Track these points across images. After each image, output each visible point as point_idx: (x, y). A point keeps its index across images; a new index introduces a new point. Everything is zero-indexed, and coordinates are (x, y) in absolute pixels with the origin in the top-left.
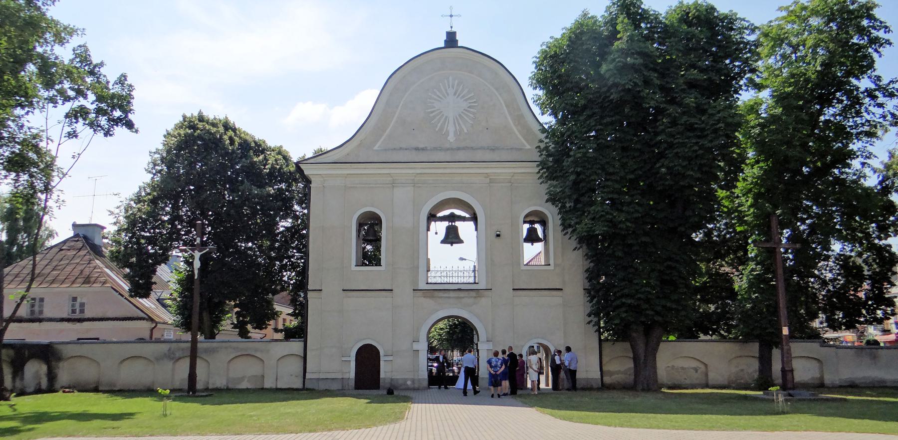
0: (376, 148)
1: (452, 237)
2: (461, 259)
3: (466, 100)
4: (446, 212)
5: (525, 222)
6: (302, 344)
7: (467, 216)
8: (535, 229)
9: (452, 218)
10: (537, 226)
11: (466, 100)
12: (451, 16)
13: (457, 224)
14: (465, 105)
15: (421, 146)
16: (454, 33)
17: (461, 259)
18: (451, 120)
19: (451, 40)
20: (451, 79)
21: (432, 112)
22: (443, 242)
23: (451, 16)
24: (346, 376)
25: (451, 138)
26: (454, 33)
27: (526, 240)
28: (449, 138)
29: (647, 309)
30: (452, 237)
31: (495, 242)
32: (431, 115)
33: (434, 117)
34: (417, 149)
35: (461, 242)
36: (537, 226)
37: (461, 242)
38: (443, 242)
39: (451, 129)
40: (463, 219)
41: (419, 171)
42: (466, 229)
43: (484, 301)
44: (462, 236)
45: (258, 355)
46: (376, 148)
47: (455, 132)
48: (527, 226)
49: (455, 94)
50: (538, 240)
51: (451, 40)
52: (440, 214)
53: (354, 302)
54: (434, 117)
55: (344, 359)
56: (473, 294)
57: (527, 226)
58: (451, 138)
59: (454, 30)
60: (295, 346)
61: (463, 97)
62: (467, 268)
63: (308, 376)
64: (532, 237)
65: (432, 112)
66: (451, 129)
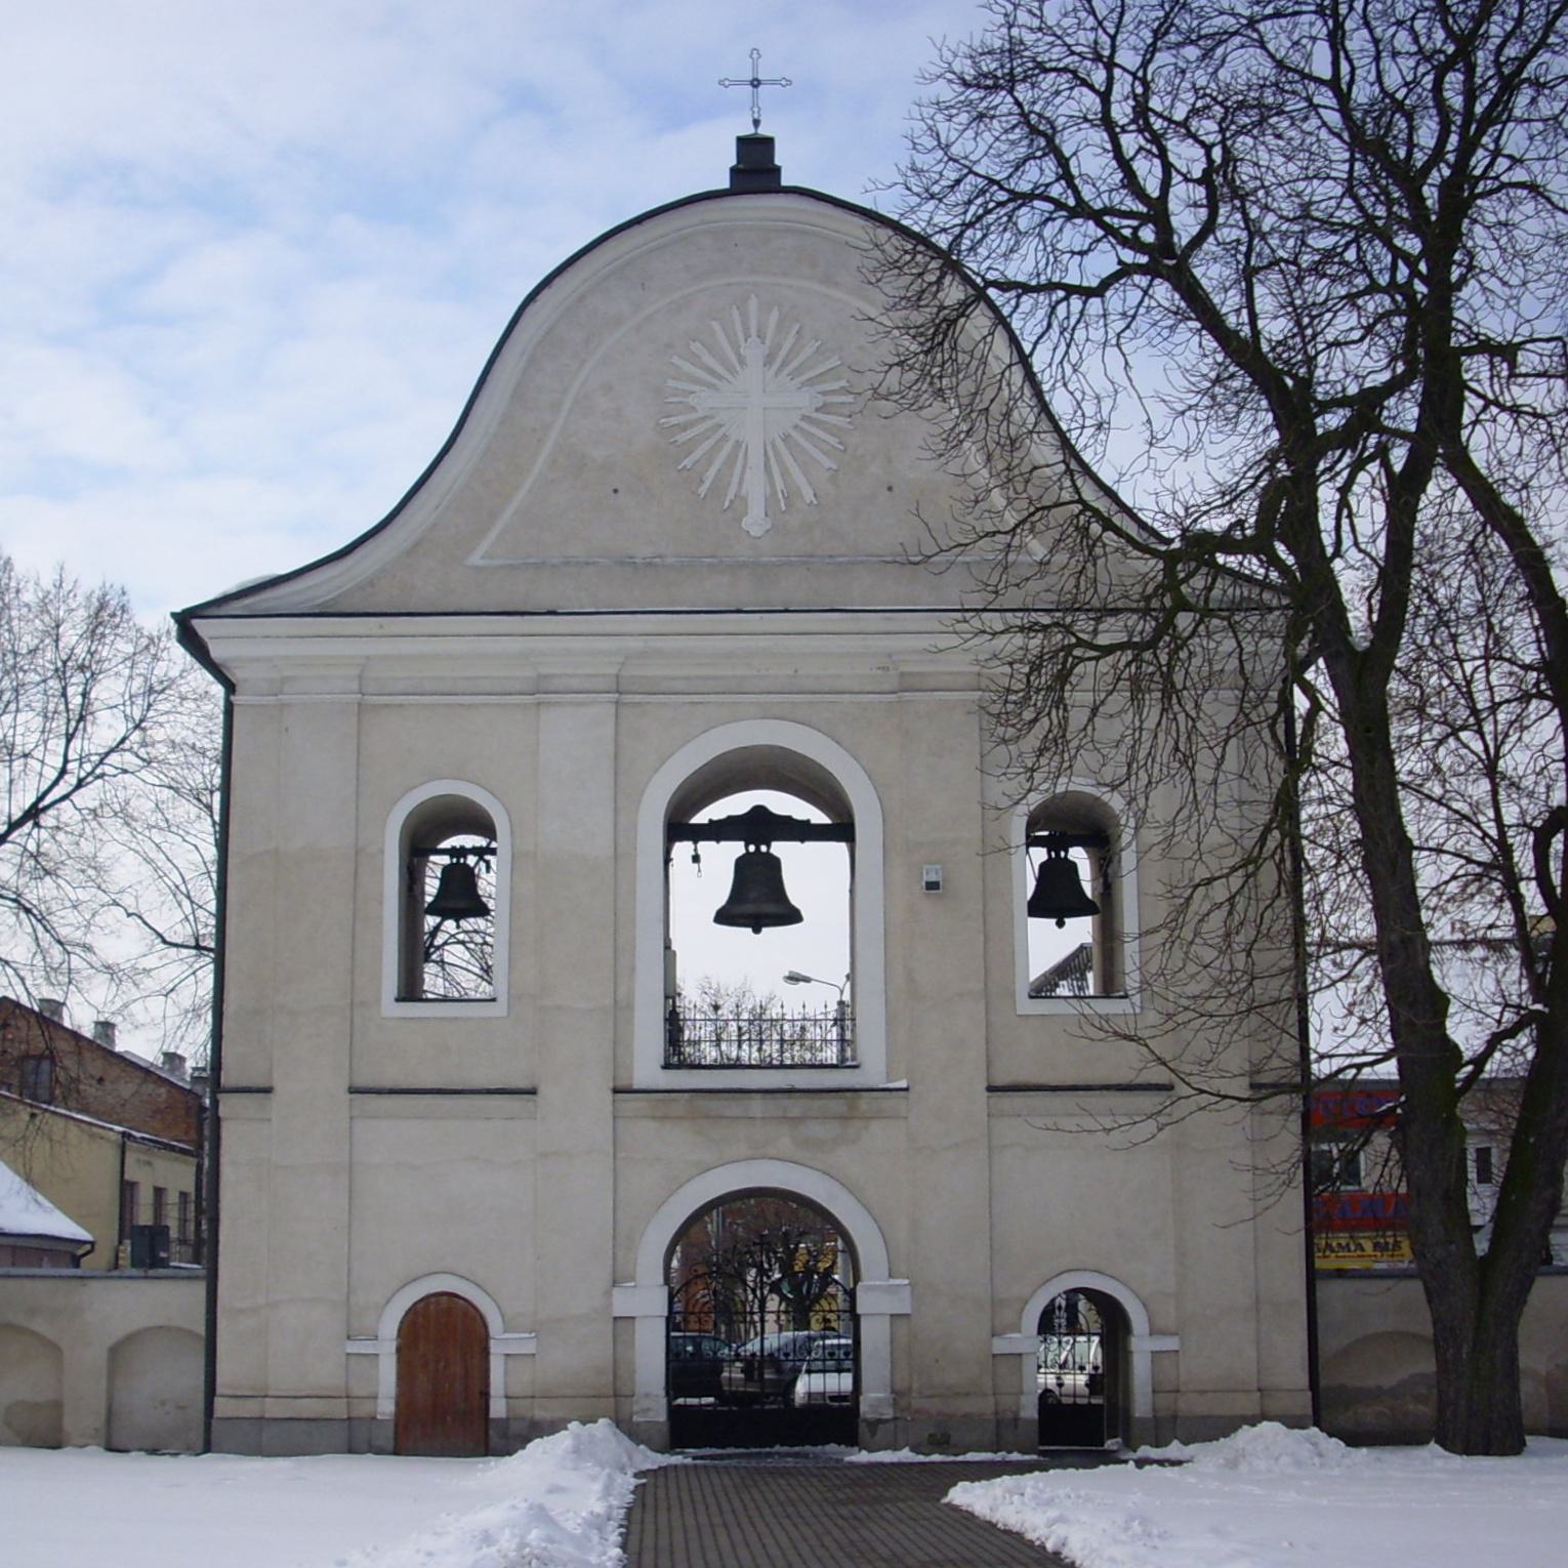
0: (475, 559)
1: (758, 901)
2: (794, 978)
3: (810, 382)
4: (737, 804)
5: (1032, 842)
6: (199, 1290)
7: (819, 817)
8: (1073, 867)
9: (760, 826)
10: (1078, 855)
11: (810, 382)
12: (756, 83)
13: (778, 848)
14: (806, 400)
15: (643, 551)
16: (768, 142)
17: (794, 978)
18: (756, 459)
19: (755, 166)
20: (753, 303)
21: (684, 428)
22: (724, 917)
23: (756, 83)
24: (362, 1410)
25: (755, 521)
26: (768, 142)
27: (1037, 908)
28: (746, 523)
29: (1496, 722)
30: (758, 901)
31: (921, 896)
32: (682, 437)
33: (693, 443)
34: (627, 562)
35: (792, 916)
36: (1078, 855)
37: (792, 916)
38: (724, 917)
39: (755, 489)
40: (802, 831)
41: (635, 644)
42: (811, 872)
43: (879, 1136)
44: (794, 895)
45: (40, 1325)
46: (475, 559)
47: (771, 500)
48: (1039, 855)
49: (769, 360)
50: (1082, 907)
51: (755, 166)
52: (701, 818)
53: (393, 1132)
54: (693, 443)
55: (353, 1347)
56: (836, 1105)
57: (1039, 855)
58: (755, 521)
59: (763, 131)
60: (169, 1301)
61: (799, 371)
62: (815, 1009)
63: (222, 1407)
64: (1056, 896)
65: (684, 428)
66: (755, 489)
